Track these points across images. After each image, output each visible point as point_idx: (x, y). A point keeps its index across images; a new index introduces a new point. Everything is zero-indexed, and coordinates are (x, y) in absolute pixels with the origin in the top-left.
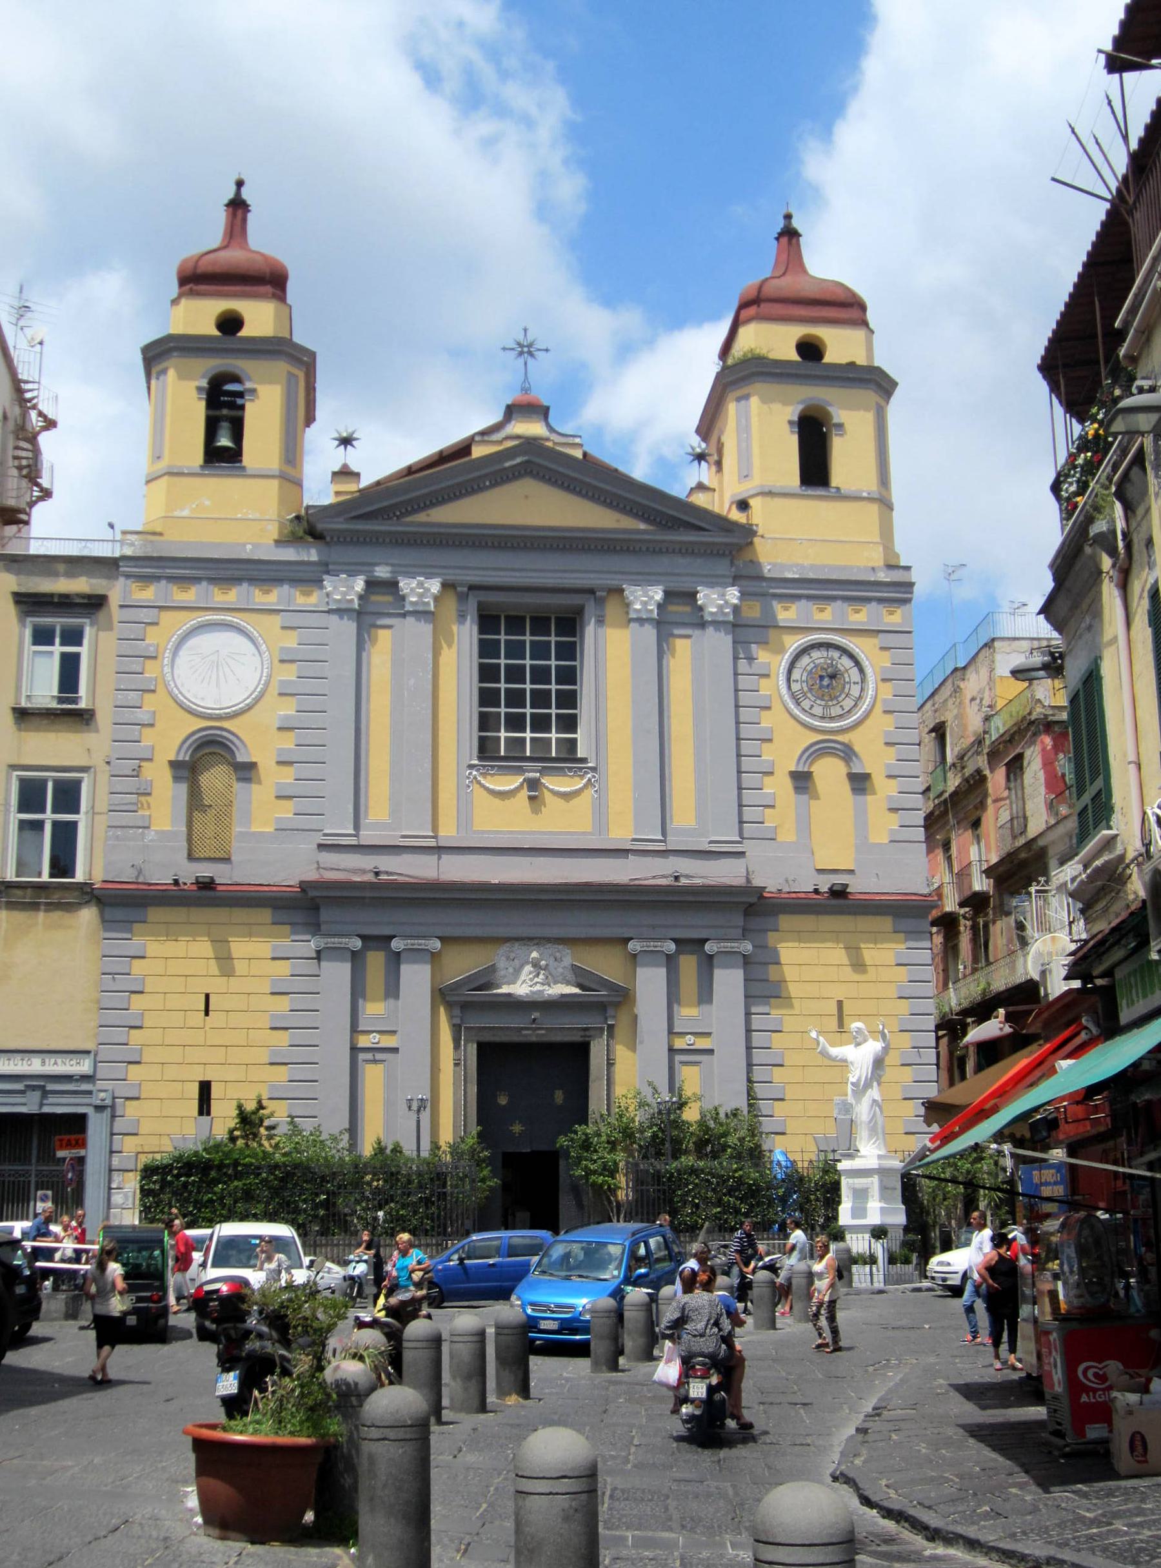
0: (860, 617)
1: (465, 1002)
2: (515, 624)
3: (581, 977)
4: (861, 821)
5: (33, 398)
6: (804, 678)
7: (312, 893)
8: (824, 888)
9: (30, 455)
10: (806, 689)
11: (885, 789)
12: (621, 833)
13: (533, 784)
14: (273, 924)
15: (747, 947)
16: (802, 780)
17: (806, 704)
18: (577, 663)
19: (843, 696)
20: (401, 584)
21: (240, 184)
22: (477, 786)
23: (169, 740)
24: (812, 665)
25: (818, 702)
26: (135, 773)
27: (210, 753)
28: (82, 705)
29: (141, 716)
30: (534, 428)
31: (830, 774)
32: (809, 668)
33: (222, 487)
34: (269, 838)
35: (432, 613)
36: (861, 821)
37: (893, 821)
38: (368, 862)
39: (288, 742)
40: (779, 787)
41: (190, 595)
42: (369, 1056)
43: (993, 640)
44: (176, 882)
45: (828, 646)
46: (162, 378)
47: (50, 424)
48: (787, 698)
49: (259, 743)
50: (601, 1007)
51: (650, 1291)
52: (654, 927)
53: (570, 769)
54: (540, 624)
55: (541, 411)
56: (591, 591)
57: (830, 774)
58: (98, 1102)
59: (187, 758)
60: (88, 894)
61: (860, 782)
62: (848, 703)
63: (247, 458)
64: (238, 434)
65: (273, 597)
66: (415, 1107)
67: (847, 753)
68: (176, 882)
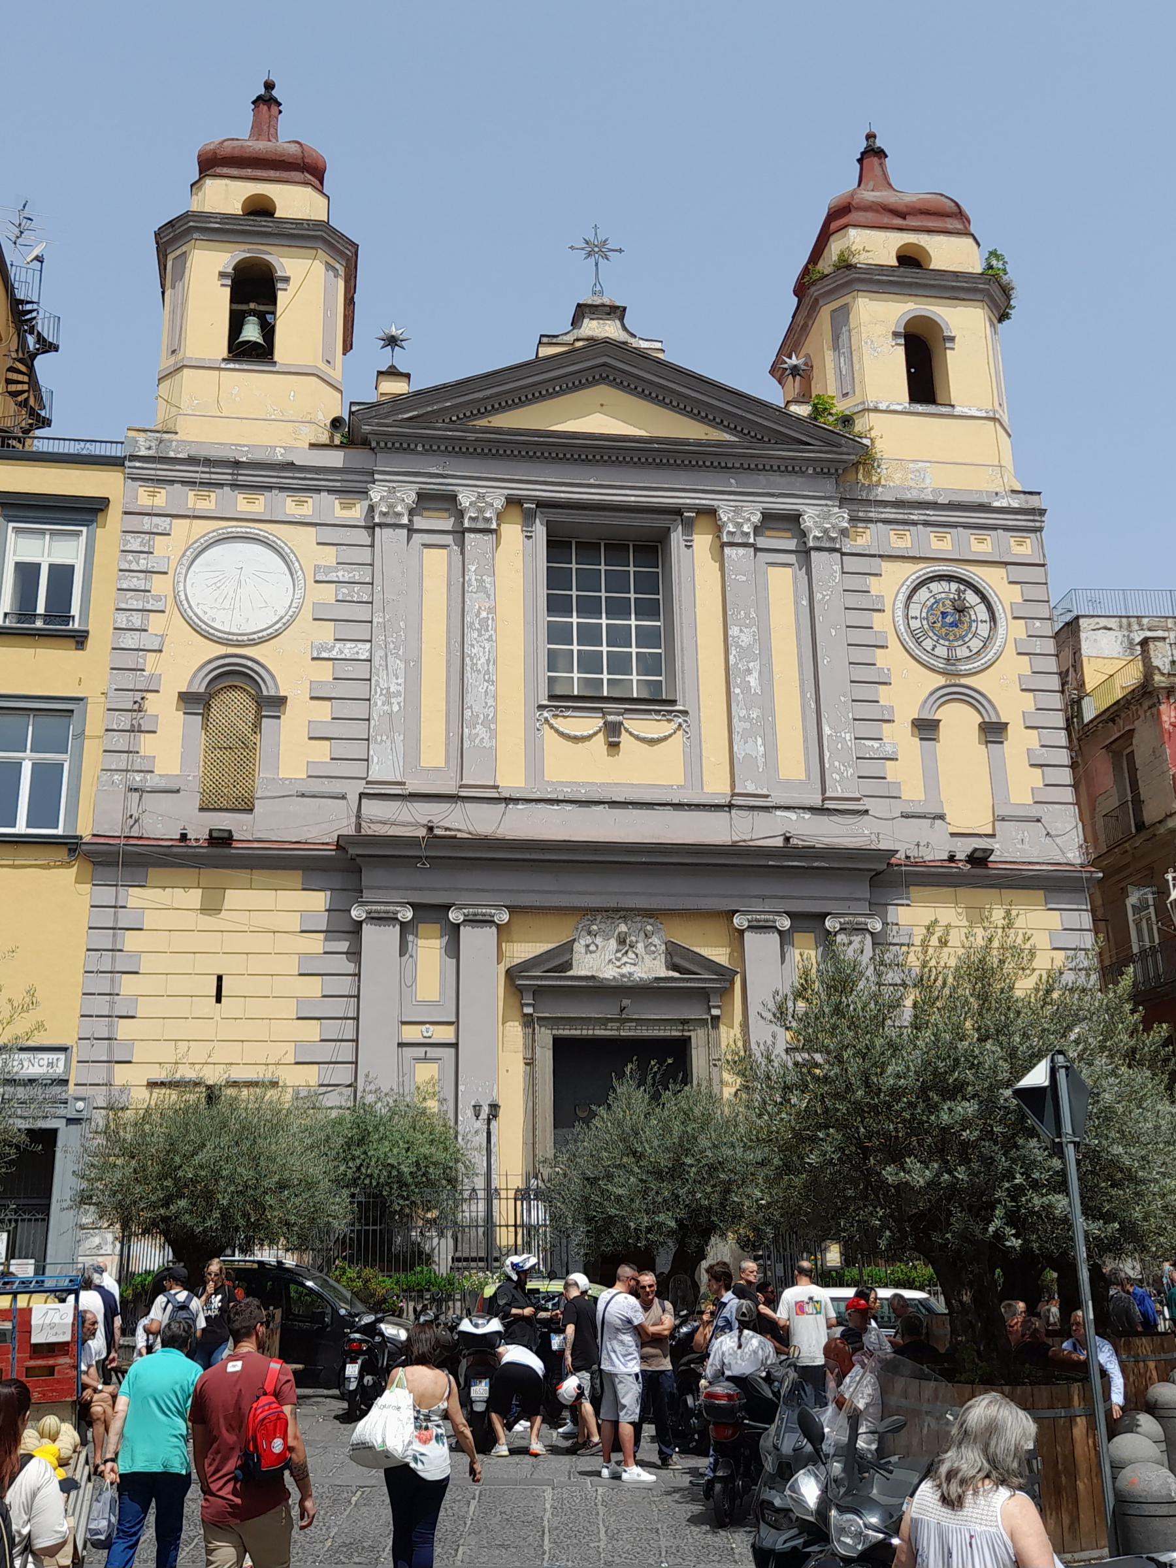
0: (981, 545)
1: (537, 989)
2: (588, 549)
3: (676, 956)
4: (998, 778)
5: (31, 311)
6: (924, 615)
7: (352, 851)
8: (960, 856)
9: (26, 379)
10: (926, 627)
11: (1020, 742)
12: (716, 787)
13: (613, 730)
14: (304, 889)
15: (876, 925)
16: (926, 728)
17: (928, 644)
18: (660, 597)
19: (970, 636)
20: (460, 497)
21: (269, 86)
22: (546, 726)
23: (182, 664)
24: (932, 600)
25: (941, 641)
26: (136, 707)
27: (235, 687)
28: (76, 625)
29: (145, 641)
30: (609, 329)
31: (960, 723)
32: (929, 604)
33: (248, 382)
34: (299, 779)
35: (495, 530)
36: (998, 778)
37: (1036, 777)
38: (424, 812)
39: (324, 672)
40: (899, 736)
41: (209, 502)
42: (420, 1052)
43: (1077, 618)
44: (184, 837)
45: (950, 578)
46: (179, 285)
47: (48, 347)
48: (906, 637)
49: (289, 669)
50: (703, 996)
51: (300, 1366)
52: (764, 898)
53: (658, 712)
54: (617, 548)
55: (616, 312)
56: (677, 512)
57: (960, 723)
58: (74, 1115)
59: (202, 690)
60: (71, 846)
61: (993, 731)
62: (976, 644)
63: (281, 352)
64: (268, 331)
65: (308, 507)
66: (484, 1115)
67: (973, 699)
68: (184, 837)
